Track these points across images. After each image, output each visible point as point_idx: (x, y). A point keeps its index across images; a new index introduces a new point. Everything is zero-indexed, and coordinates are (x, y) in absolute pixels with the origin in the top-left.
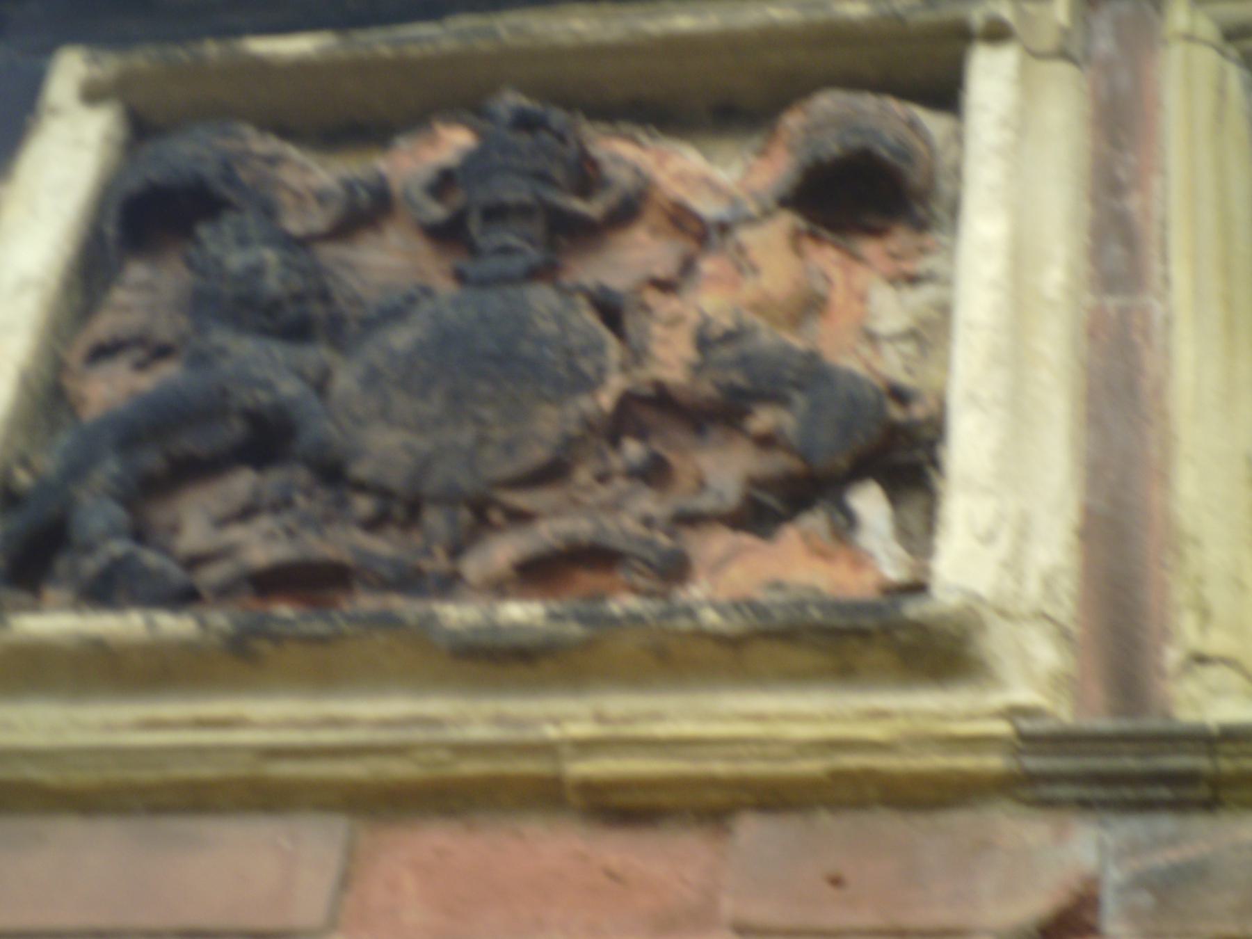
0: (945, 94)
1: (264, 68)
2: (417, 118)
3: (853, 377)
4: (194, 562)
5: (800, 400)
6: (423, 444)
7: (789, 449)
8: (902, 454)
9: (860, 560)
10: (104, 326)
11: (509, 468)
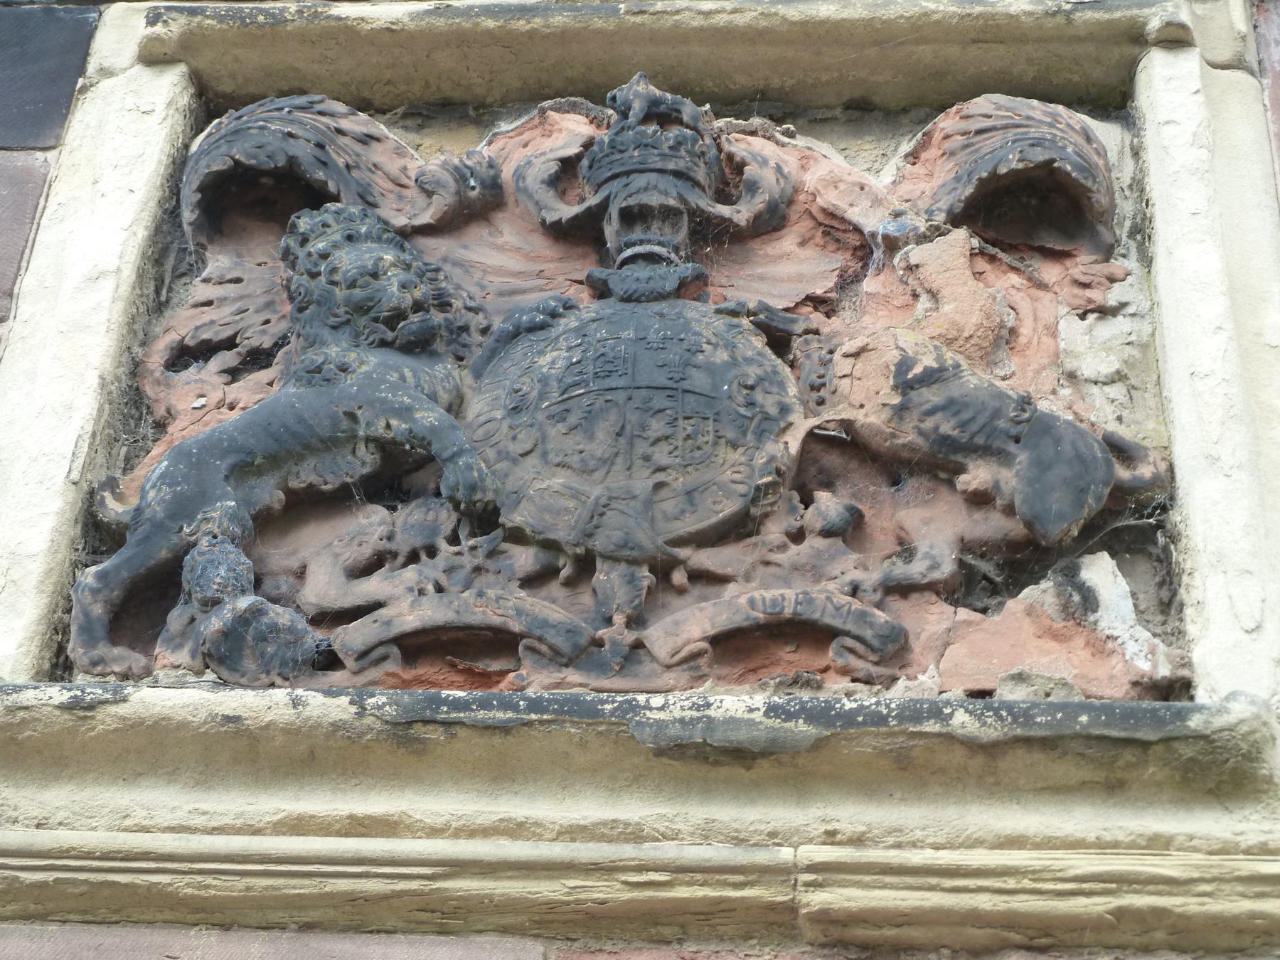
0: (1114, 101)
2: (531, 96)
5: (1023, 457)
6: (596, 492)
7: (1009, 510)
9: (1102, 646)
10: (184, 324)
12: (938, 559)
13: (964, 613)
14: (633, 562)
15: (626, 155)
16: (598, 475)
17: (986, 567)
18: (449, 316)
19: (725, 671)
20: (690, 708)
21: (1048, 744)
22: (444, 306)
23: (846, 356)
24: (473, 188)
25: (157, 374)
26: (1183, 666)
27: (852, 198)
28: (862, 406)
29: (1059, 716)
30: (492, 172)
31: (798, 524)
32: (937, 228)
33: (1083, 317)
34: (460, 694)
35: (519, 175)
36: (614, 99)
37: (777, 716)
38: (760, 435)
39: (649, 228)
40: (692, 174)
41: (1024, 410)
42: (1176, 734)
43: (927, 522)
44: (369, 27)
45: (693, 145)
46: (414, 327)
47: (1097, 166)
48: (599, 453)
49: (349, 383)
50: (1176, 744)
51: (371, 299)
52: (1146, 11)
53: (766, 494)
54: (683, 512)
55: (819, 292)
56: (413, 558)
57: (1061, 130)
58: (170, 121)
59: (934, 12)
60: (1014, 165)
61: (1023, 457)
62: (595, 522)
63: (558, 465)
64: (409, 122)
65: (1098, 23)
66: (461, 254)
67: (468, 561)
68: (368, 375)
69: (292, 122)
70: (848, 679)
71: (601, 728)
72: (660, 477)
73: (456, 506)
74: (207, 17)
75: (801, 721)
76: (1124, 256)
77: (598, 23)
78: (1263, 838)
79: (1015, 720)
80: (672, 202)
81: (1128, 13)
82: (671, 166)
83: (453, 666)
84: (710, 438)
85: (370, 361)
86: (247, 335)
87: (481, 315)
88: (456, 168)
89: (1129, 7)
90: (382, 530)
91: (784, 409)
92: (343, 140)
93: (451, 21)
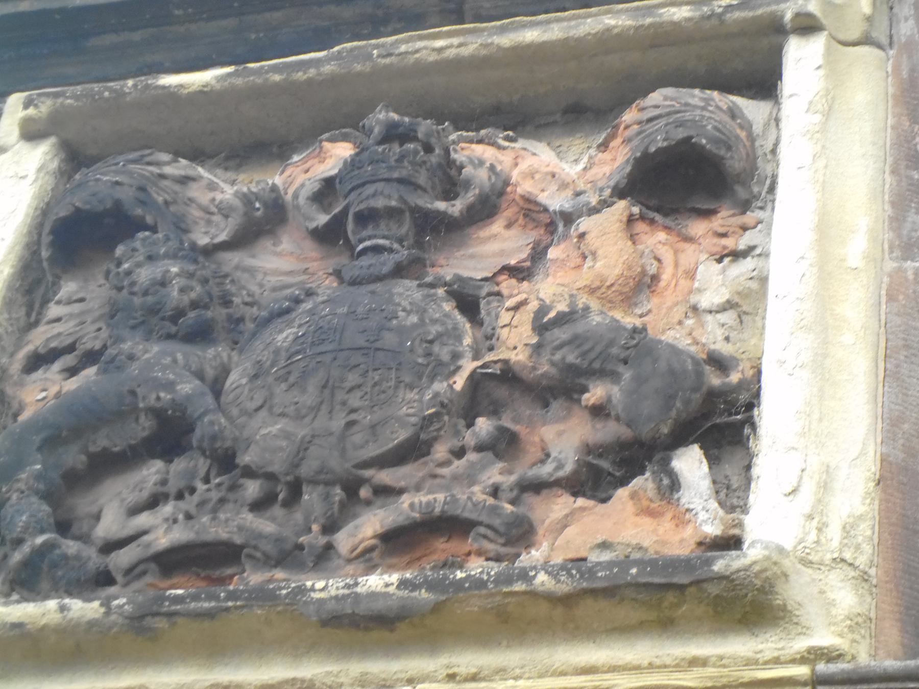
0: (764, 83)
1: (172, 96)
3: (674, 350)
4: (110, 547)
5: (627, 374)
6: (302, 432)
7: (618, 419)
8: (720, 418)
9: (683, 518)
10: (38, 339)
11: (372, 451)
12: (563, 462)
13: (581, 502)
14: (327, 483)
15: (363, 170)
16: (307, 420)
17: (605, 464)
18: (230, 311)
19: (394, 561)
20: (343, 588)
21: (610, 592)
22: (226, 302)
23: (508, 310)
24: (258, 209)
25: (15, 377)
26: (735, 526)
27: (543, 185)
28: (515, 348)
29: (615, 570)
30: (274, 195)
31: (460, 444)
32: (605, 201)
33: (719, 261)
34: (180, 592)
35: (296, 196)
36: (364, 126)
37: (406, 588)
38: (432, 378)
39: (378, 226)
40: (413, 180)
41: (633, 338)
42: (704, 577)
43: (560, 434)
44: (186, 91)
45: (415, 157)
46: (191, 322)
47: (737, 137)
48: (309, 403)
49: (134, 369)
50: (705, 585)
51: (158, 303)
52: (782, 6)
53: (432, 423)
54: (367, 442)
55: (513, 262)
56: (180, 496)
57: (711, 112)
58: (40, 182)
59: (615, 27)
60: (660, 145)
61: (627, 374)
62: (301, 455)
63: (279, 415)
64: (231, 163)
65: (745, 20)
66: (250, 262)
67: (215, 495)
68: (148, 360)
69: (123, 173)
70: (483, 558)
71: (280, 608)
72: (354, 416)
73: (203, 453)
74: (67, 98)
75: (423, 591)
76: (761, 208)
77: (358, 67)
78: (776, 654)
79: (582, 576)
80: (394, 203)
81: (769, 9)
82: (396, 175)
83: (198, 575)
84: (392, 383)
85: (152, 351)
86: (84, 341)
87: (255, 309)
88: (244, 195)
89: (769, 4)
90: (155, 478)
91: (456, 356)
92: (166, 183)
93: (246, 79)
